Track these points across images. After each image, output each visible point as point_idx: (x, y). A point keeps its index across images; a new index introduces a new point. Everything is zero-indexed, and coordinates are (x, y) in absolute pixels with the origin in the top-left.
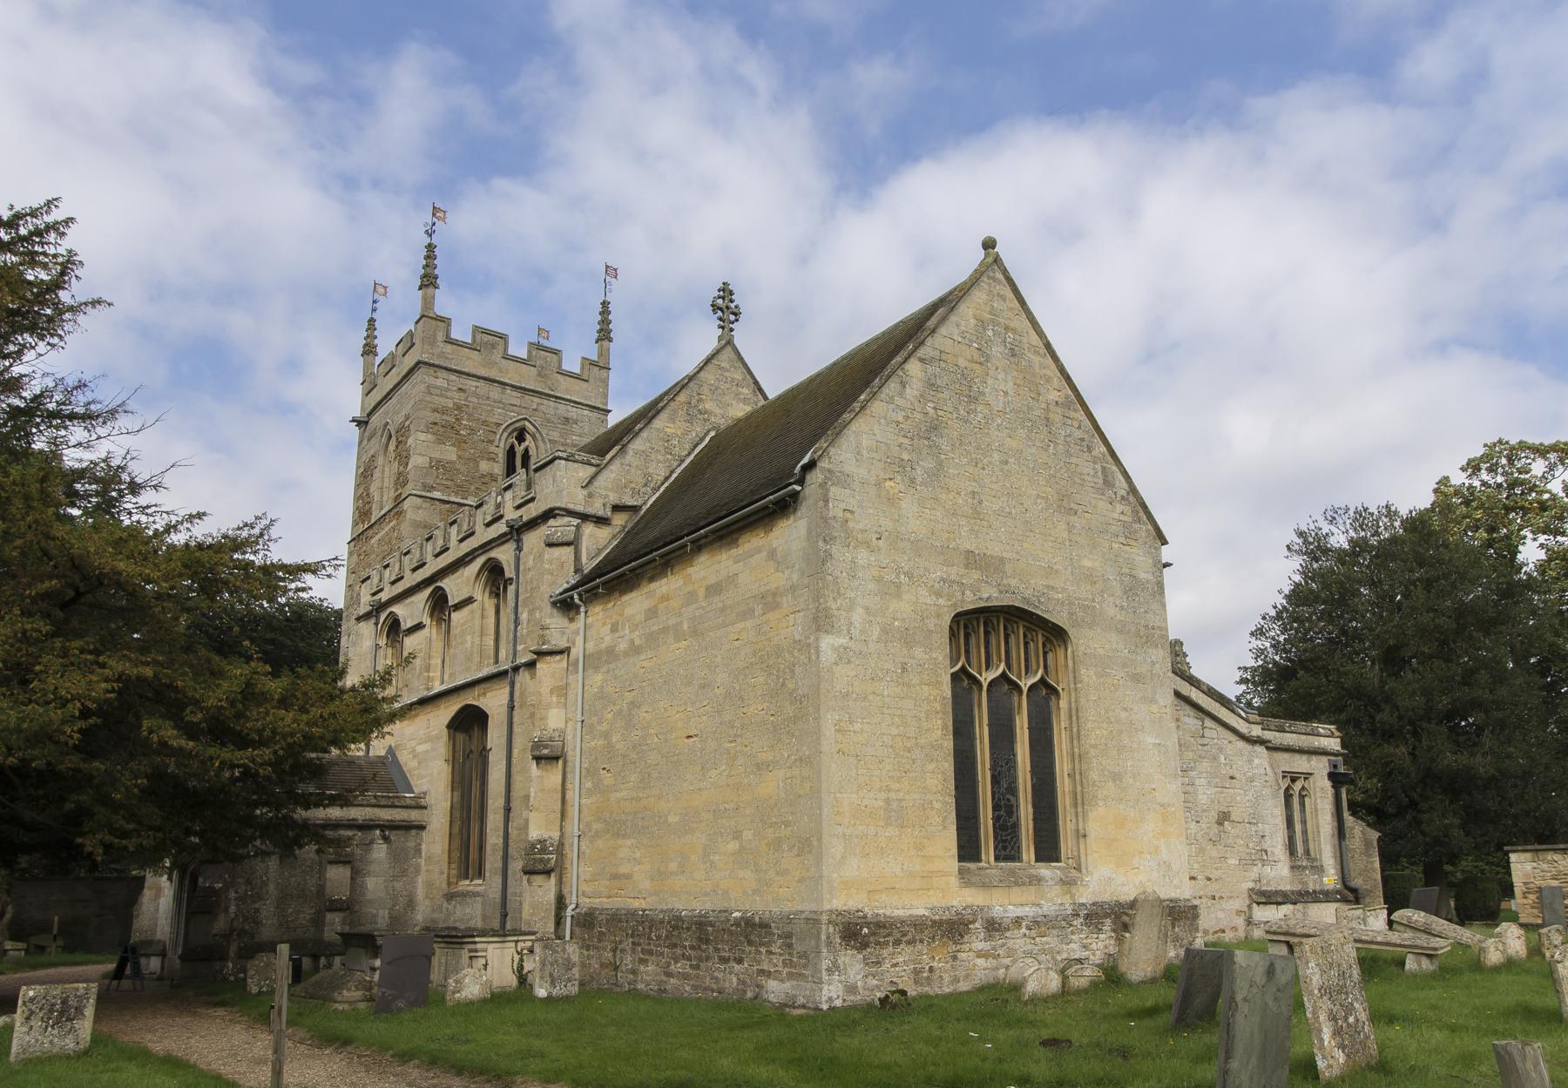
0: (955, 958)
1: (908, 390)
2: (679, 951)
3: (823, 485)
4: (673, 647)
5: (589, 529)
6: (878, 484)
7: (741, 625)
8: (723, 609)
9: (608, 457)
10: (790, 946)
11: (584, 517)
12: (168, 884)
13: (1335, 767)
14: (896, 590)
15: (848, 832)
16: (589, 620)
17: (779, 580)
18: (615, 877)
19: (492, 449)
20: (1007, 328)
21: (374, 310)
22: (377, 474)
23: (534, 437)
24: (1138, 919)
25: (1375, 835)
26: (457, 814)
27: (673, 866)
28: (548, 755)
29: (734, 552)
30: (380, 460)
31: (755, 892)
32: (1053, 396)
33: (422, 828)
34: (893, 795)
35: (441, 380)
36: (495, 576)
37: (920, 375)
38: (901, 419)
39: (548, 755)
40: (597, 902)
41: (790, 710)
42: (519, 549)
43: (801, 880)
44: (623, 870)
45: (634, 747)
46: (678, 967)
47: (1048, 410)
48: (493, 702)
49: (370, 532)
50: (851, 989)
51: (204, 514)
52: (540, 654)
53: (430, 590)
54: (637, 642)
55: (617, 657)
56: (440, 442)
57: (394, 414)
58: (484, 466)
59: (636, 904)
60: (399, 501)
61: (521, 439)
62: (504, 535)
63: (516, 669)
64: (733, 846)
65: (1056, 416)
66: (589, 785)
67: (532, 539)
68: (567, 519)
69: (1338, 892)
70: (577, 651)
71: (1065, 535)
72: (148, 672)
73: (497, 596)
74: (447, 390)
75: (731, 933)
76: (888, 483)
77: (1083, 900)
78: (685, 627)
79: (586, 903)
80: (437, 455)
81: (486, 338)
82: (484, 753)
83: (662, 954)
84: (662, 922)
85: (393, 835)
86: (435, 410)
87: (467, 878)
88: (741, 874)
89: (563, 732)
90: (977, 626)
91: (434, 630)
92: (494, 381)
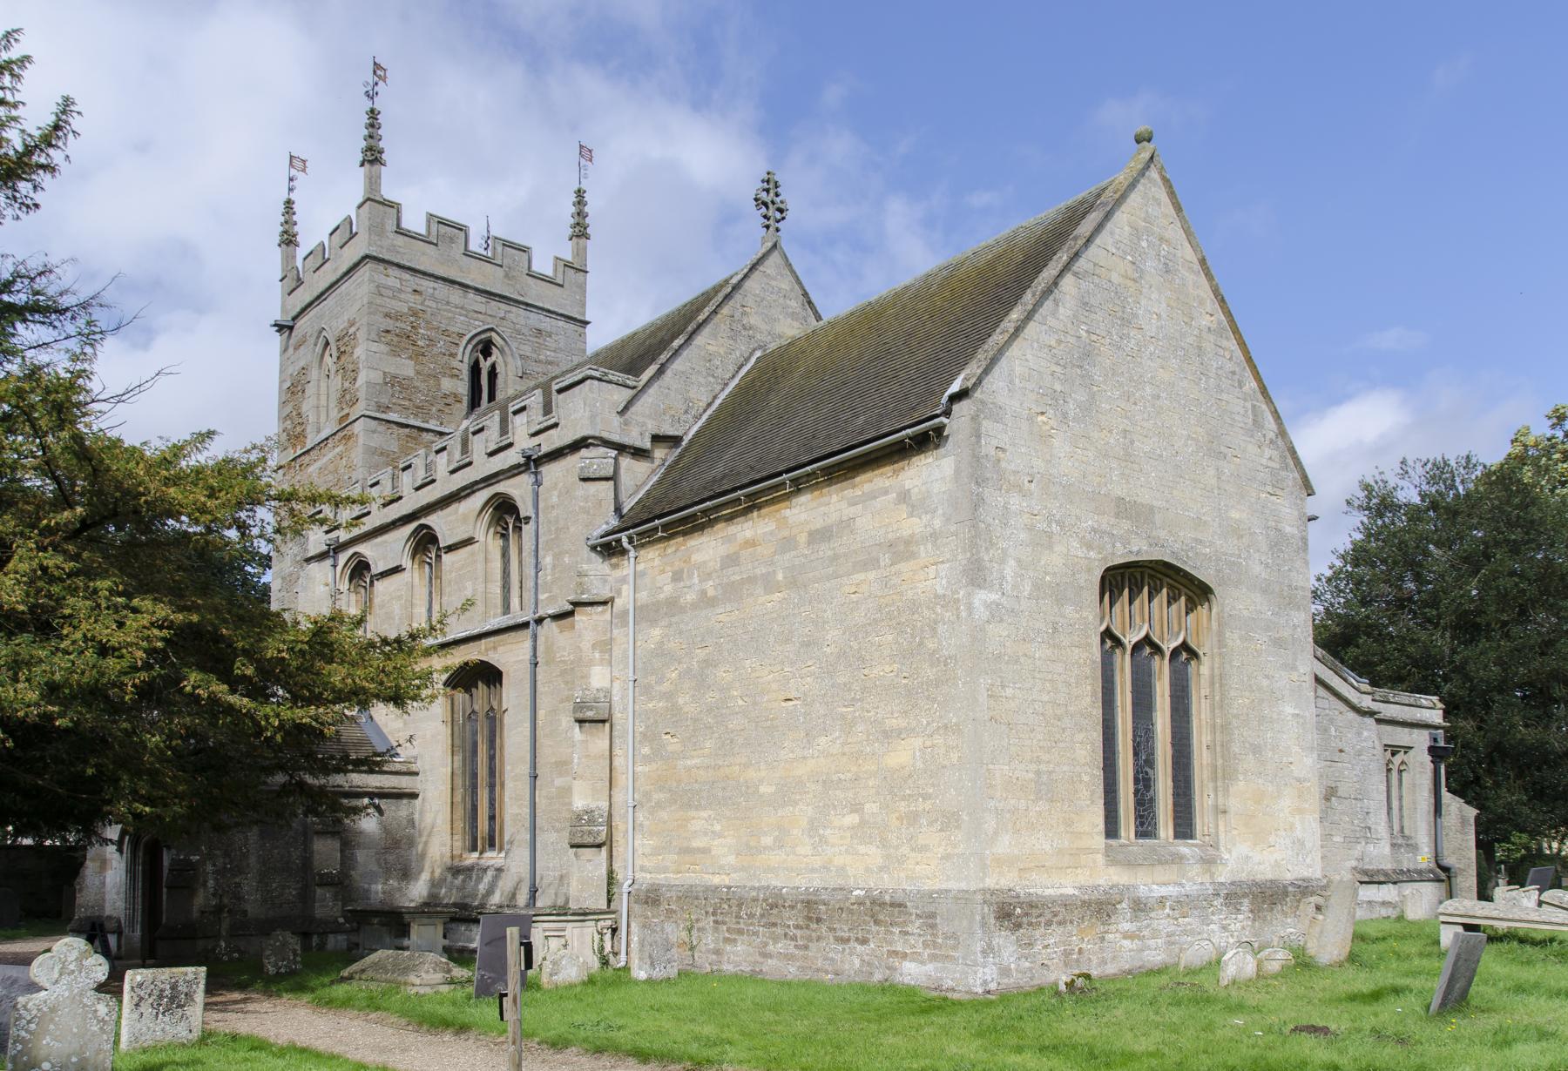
0: (1103, 939)
1: (1061, 310)
2: (779, 930)
3: (975, 418)
4: (761, 600)
5: (626, 462)
6: (1030, 419)
7: (861, 576)
8: (835, 557)
9: (645, 376)
10: (933, 926)
11: (621, 448)
12: (117, 855)
13: (1435, 740)
14: (1044, 541)
15: (1001, 805)
16: (640, 567)
17: (912, 526)
18: (687, 851)
19: (455, 364)
20: (1161, 239)
21: (291, 190)
22: (310, 390)
23: (502, 351)
24: (1332, 901)
25: (1472, 812)
26: (459, 781)
27: (767, 840)
28: (593, 719)
29: (849, 493)
30: (314, 374)
31: (881, 869)
32: (1206, 321)
33: (414, 796)
34: (1043, 767)
35: (393, 278)
36: (504, 512)
37: (1074, 291)
38: (1053, 343)
39: (593, 719)
40: (660, 878)
41: (930, 672)
42: (538, 483)
43: (946, 857)
44: (696, 843)
45: (710, 710)
46: (781, 946)
47: (1199, 337)
48: (509, 656)
49: (306, 459)
50: (1005, 971)
51: (214, 433)
52: (576, 604)
53: (414, 525)
54: (711, 593)
55: (683, 610)
56: (395, 353)
57: (331, 318)
58: (447, 384)
59: (716, 880)
60: (345, 424)
61: (486, 352)
62: (519, 466)
63: (539, 621)
64: (853, 819)
65: (1208, 346)
66: (646, 750)
67: (550, 471)
68: (602, 450)
69: (1431, 871)
70: (624, 601)
71: (1214, 481)
72: (195, 618)
73: (504, 536)
74: (400, 291)
75: (851, 912)
76: (1040, 418)
77: (1222, 880)
78: (780, 576)
79: (645, 879)
80: (392, 370)
81: (444, 229)
82: (494, 721)
83: (756, 934)
84: (755, 900)
85: (383, 803)
86: (387, 315)
87: (474, 848)
88: (862, 849)
89: (608, 693)
90: (1123, 580)
91: (416, 575)
92: (453, 282)
